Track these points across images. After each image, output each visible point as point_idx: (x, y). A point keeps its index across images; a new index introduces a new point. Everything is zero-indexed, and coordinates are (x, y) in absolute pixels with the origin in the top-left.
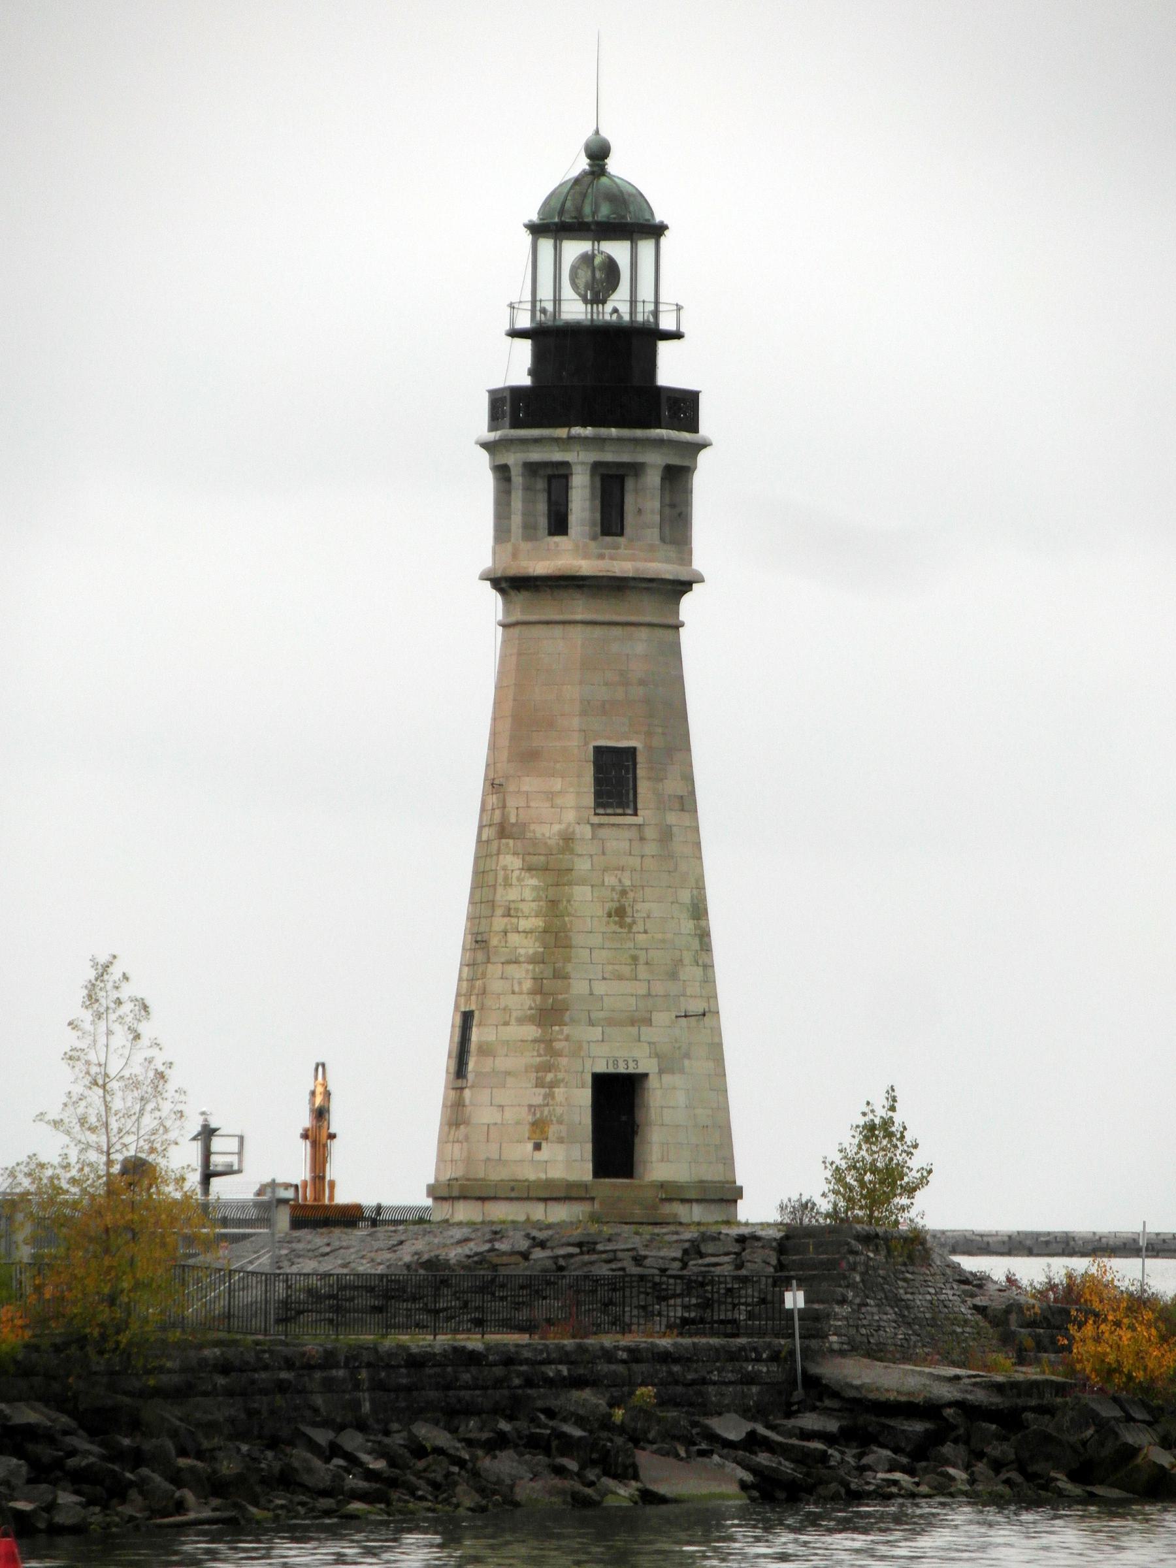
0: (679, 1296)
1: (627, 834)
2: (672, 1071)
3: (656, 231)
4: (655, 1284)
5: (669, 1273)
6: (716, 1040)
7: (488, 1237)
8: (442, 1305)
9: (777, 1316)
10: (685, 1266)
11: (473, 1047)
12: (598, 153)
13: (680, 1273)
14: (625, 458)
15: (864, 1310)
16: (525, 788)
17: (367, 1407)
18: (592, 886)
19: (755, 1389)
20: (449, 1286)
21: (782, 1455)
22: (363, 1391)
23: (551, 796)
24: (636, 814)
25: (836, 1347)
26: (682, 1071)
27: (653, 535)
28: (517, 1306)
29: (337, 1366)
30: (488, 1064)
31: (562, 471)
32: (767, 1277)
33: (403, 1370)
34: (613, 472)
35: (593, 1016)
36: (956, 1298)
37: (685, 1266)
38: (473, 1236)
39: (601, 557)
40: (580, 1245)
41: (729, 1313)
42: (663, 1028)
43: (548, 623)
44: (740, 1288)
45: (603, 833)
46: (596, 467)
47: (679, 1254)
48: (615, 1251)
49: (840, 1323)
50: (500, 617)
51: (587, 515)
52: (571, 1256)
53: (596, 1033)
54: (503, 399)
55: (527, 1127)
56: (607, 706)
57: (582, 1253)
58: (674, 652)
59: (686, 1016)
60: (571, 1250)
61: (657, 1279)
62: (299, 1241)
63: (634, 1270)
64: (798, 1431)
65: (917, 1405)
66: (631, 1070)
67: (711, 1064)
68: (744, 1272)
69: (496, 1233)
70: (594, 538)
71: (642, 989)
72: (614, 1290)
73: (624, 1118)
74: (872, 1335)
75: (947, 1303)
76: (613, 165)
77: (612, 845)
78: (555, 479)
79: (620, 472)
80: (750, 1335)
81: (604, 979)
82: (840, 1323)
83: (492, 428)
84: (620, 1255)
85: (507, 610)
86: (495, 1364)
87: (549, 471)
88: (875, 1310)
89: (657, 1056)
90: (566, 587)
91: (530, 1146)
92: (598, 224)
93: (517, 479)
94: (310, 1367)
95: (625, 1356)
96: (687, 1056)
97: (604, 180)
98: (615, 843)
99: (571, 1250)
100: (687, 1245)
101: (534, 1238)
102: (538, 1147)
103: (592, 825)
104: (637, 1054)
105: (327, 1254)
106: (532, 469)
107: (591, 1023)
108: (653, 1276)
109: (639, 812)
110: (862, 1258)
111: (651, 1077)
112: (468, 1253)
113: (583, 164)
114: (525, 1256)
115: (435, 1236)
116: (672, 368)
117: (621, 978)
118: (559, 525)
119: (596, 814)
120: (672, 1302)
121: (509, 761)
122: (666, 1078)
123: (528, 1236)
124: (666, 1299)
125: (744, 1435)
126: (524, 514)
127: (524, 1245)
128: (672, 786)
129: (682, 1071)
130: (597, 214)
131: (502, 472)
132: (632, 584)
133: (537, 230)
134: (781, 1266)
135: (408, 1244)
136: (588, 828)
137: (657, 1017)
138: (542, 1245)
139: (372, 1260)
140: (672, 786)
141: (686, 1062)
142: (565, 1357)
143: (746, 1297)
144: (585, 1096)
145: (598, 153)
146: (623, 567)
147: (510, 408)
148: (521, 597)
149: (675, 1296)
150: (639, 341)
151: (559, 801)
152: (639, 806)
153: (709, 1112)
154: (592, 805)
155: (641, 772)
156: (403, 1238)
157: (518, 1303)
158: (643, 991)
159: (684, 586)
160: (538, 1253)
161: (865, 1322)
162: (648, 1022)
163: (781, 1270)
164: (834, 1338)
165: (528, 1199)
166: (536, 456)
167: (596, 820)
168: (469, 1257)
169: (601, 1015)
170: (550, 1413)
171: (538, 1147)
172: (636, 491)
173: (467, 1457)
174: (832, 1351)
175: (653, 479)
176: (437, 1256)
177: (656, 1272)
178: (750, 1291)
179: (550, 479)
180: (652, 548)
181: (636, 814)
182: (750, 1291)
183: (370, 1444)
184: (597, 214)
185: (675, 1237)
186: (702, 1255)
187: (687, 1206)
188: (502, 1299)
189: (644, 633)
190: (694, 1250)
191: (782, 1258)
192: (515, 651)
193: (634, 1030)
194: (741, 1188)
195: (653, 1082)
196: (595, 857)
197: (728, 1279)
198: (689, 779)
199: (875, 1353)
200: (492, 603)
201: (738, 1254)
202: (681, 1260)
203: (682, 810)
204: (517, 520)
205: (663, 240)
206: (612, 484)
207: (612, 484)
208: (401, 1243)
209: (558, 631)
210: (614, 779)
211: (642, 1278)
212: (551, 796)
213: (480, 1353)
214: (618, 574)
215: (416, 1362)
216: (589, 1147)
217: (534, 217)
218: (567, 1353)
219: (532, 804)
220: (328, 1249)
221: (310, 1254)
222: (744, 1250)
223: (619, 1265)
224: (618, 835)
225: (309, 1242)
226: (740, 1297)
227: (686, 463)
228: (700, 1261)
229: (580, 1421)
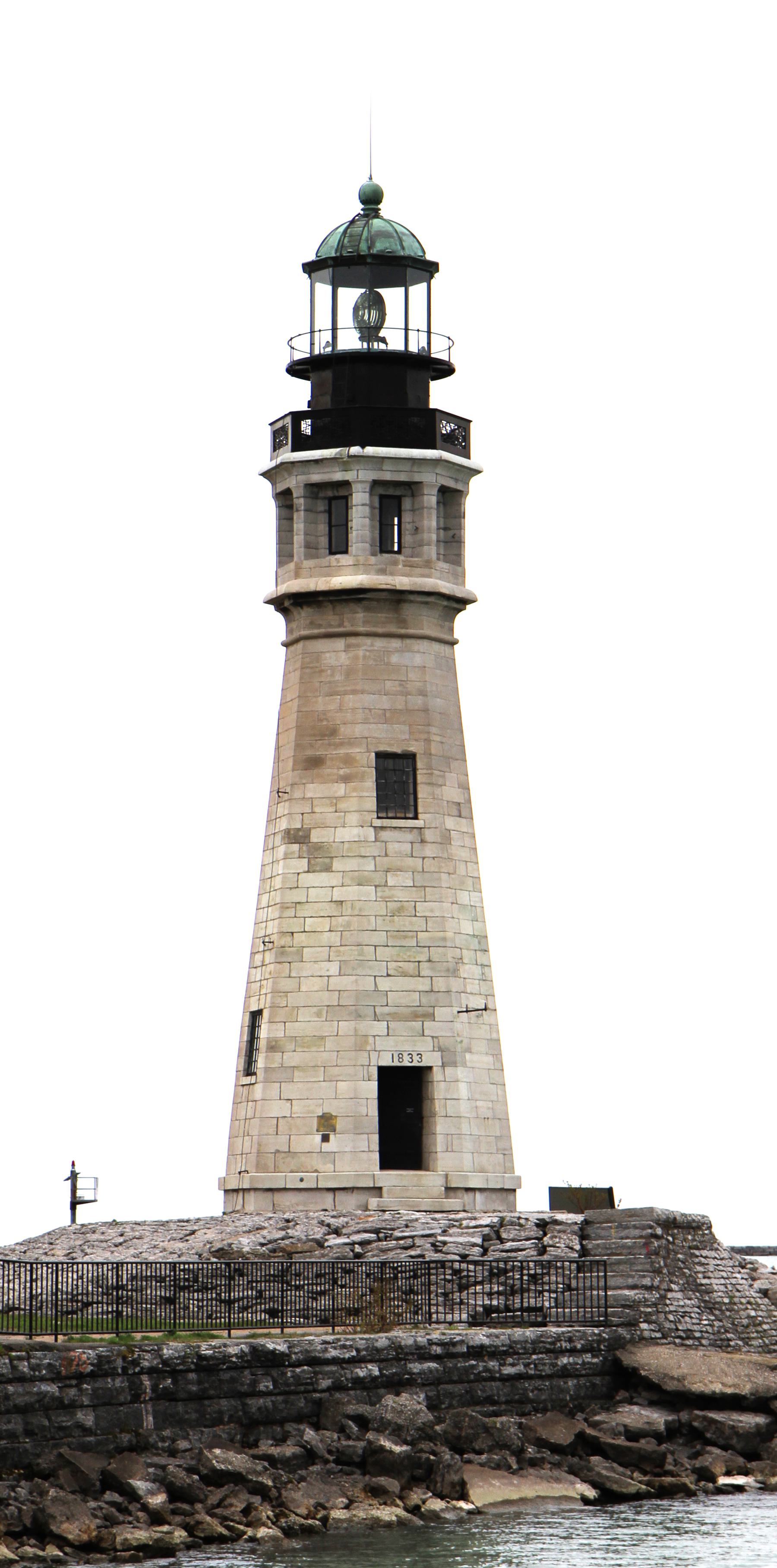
0: (481, 1283)
1: (409, 837)
2: (454, 1064)
4: (456, 1272)
5: (468, 1259)
6: (494, 1036)
7: (281, 1225)
8: (235, 1295)
9: (588, 1303)
10: (485, 1252)
11: (262, 1044)
12: (372, 199)
13: (481, 1259)
15: (670, 1295)
16: (309, 795)
17: (149, 1421)
18: (376, 886)
19: (571, 1383)
20: (242, 1275)
21: (614, 1461)
22: (145, 1402)
23: (334, 801)
24: (416, 817)
25: (646, 1334)
26: (464, 1064)
27: (431, 551)
28: (316, 1296)
29: (113, 1374)
31: (342, 492)
32: (571, 1262)
33: (192, 1376)
34: (391, 492)
35: (378, 1010)
36: (744, 1282)
37: (485, 1252)
38: (266, 1225)
39: (382, 571)
40: (377, 1231)
41: (532, 1301)
42: (447, 1023)
44: (543, 1274)
45: (385, 835)
46: (376, 484)
47: (479, 1241)
48: (412, 1237)
49: (649, 1310)
51: (367, 533)
52: (369, 1242)
53: (380, 1027)
54: (283, 429)
55: (315, 1121)
56: (388, 715)
57: (379, 1240)
58: (449, 667)
59: (467, 1011)
60: (366, 1236)
61: (456, 1266)
62: (94, 1232)
63: (431, 1256)
64: (622, 1429)
65: (742, 1398)
66: (415, 1064)
67: (490, 1059)
68: (546, 1257)
69: (288, 1221)
70: (373, 554)
71: (423, 985)
72: (415, 1277)
73: (409, 1110)
74: (680, 1322)
75: (738, 1287)
76: (385, 209)
77: (393, 847)
78: (332, 499)
79: (398, 492)
80: (558, 1324)
81: (388, 975)
82: (649, 1310)
84: (418, 1242)
85: (289, 631)
86: (299, 1364)
87: (330, 493)
88: (679, 1295)
89: (441, 1050)
90: (347, 601)
91: (318, 1138)
92: (373, 256)
93: (300, 502)
94: (81, 1377)
95: (438, 1350)
96: (469, 1050)
97: (376, 222)
98: (397, 845)
99: (366, 1236)
100: (486, 1230)
101: (329, 1225)
102: (325, 1139)
103: (375, 827)
104: (420, 1048)
105: (121, 1244)
106: (314, 490)
107: (376, 1018)
108: (453, 1261)
109: (420, 816)
110: (664, 1242)
111: (435, 1069)
112: (262, 1241)
113: (357, 208)
114: (320, 1244)
115: (228, 1225)
117: (405, 974)
118: (338, 544)
119: (378, 818)
120: (472, 1290)
121: (293, 770)
122: (449, 1070)
123: (322, 1223)
124: (467, 1287)
125: (573, 1437)
126: (306, 534)
127: (318, 1233)
128: (451, 793)
129: (464, 1064)
131: (284, 499)
132: (412, 597)
133: (310, 268)
134: (584, 1252)
135: (199, 1233)
136: (372, 829)
137: (439, 1012)
138: (337, 1232)
139: (165, 1250)
140: (451, 793)
141: (468, 1056)
142: (374, 1355)
143: (549, 1284)
144: (372, 1087)
145: (372, 199)
146: (402, 582)
147: (287, 432)
148: (304, 614)
149: (476, 1283)
151: (342, 806)
152: (420, 810)
153: (490, 1105)
154: (375, 808)
155: (420, 778)
156: (196, 1228)
157: (317, 1293)
158: (428, 988)
159: (461, 603)
160: (334, 1241)
161: (672, 1308)
162: (432, 1017)
163: (584, 1255)
164: (644, 1326)
165: (333, 1190)
166: (316, 477)
167: (378, 823)
168: (262, 1245)
169: (386, 1010)
170: (363, 1422)
171: (325, 1139)
172: (413, 510)
173: (270, 1483)
174: (642, 1338)
175: (431, 499)
176: (230, 1245)
177: (457, 1258)
178: (553, 1278)
180: (428, 564)
181: (416, 817)
182: (553, 1278)
183: (151, 1470)
185: (473, 1223)
186: (502, 1241)
187: (471, 1194)
188: (298, 1288)
189: (424, 645)
190: (494, 1234)
191: (584, 1242)
192: (298, 665)
193: (417, 1025)
194: (519, 1178)
195: (437, 1075)
196: (377, 858)
197: (532, 1265)
198: (465, 787)
199: (687, 1339)
200: (276, 624)
201: (540, 1239)
202: (482, 1246)
203: (460, 816)
204: (298, 539)
205: (433, 281)
206: (392, 499)
207: (392, 499)
208: (193, 1232)
209: (340, 643)
210: (397, 784)
211: (442, 1264)
212: (334, 801)
213: (282, 1354)
214: (398, 588)
215: (208, 1367)
216: (376, 1138)
217: (311, 257)
218: (378, 1350)
219: (316, 810)
220: (121, 1240)
221: (104, 1245)
222: (545, 1234)
223: (418, 1252)
224: (398, 837)
225: (103, 1233)
226: (543, 1283)
227: (459, 487)
228: (500, 1247)
229: (398, 1432)
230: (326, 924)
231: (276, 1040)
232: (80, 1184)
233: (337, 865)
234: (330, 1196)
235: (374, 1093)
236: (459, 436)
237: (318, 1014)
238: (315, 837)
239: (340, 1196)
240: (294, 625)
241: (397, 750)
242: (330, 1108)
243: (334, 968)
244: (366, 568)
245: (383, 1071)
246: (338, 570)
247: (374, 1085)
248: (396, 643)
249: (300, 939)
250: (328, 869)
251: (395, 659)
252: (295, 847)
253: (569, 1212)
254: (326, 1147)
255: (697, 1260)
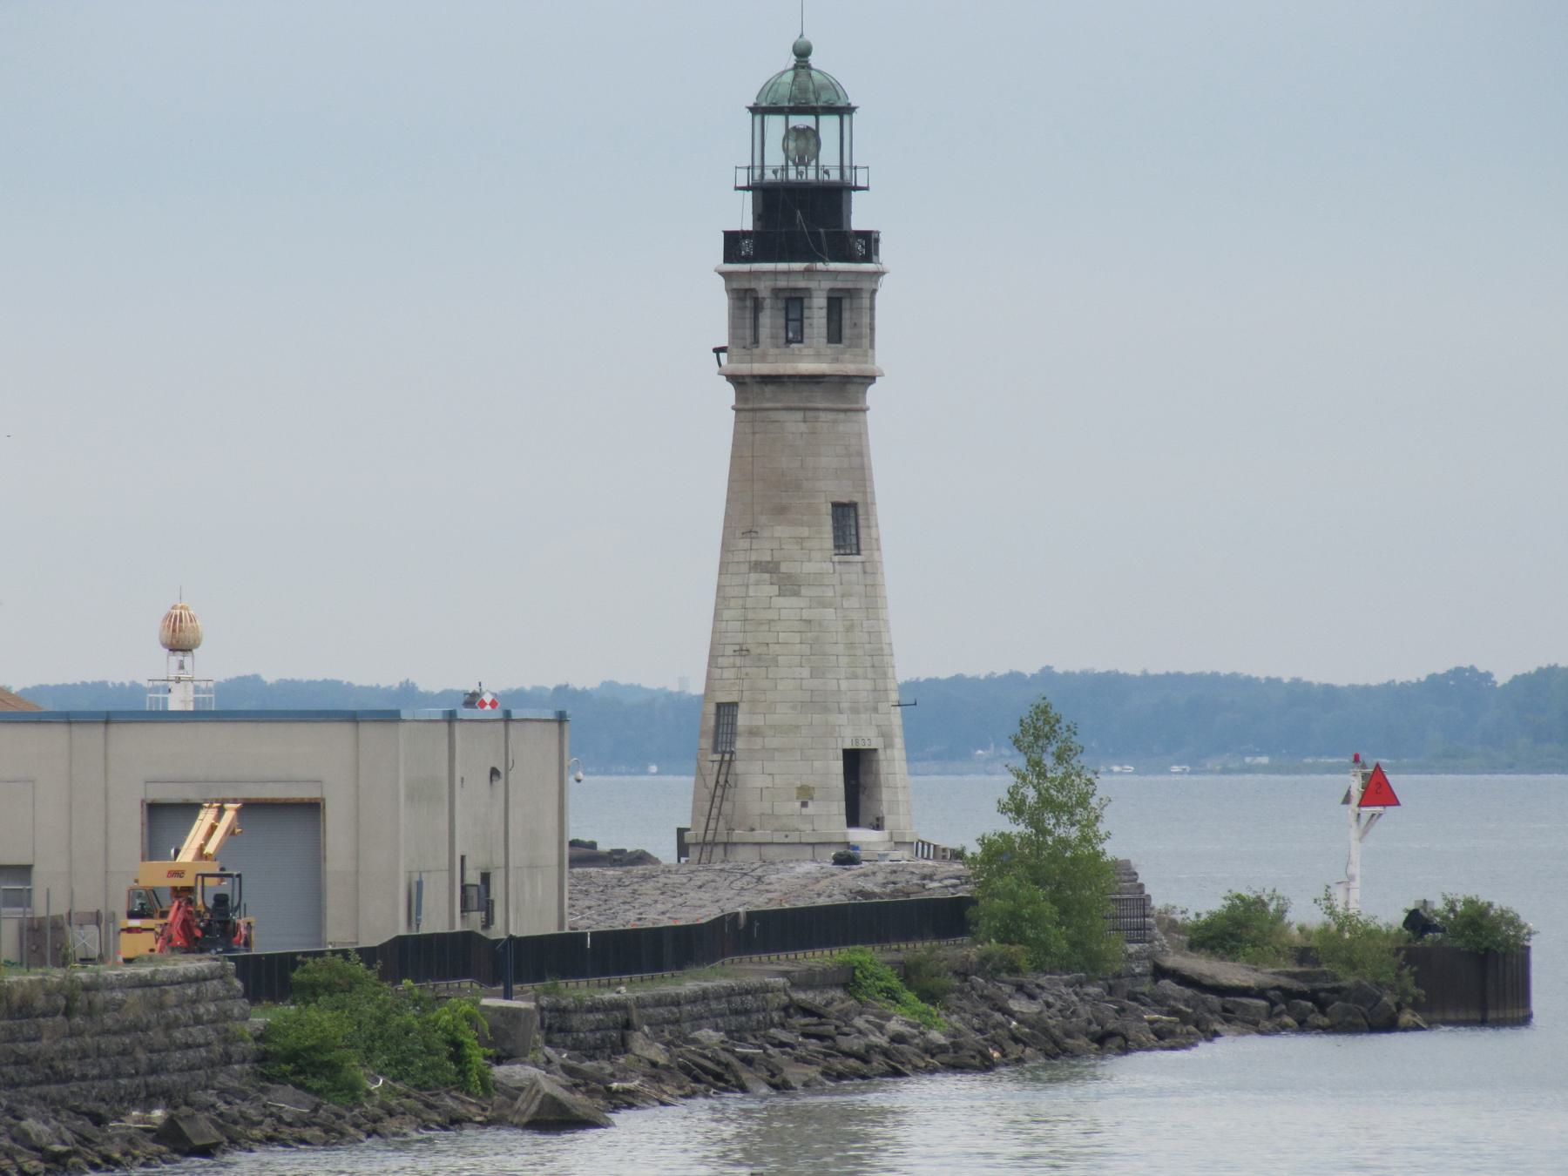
3: (848, 110)
12: (802, 53)
14: (850, 285)
16: (776, 535)
23: (800, 540)
30: (758, 743)
39: (836, 360)
43: (791, 409)
50: (733, 402)
76: (813, 60)
83: (727, 259)
87: (787, 295)
91: (798, 804)
102: (804, 804)
107: (840, 712)
116: (861, 215)
130: (804, 99)
133: (759, 110)
145: (802, 53)
150: (834, 197)
151: (807, 544)
159: (871, 379)
165: (813, 844)
171: (804, 804)
172: (851, 309)
179: (789, 300)
184: (804, 99)
195: (881, 755)
209: (799, 415)
212: (800, 540)
230: (797, 638)
231: (758, 727)
232: (754, 775)
233: (804, 591)
234: (809, 849)
235: (841, 770)
236: (868, 244)
237: (794, 708)
238: (784, 568)
239: (818, 849)
240: (746, 400)
241: (845, 500)
242: (809, 781)
243: (806, 673)
244: (818, 356)
245: (846, 752)
246: (801, 358)
247: (841, 763)
248: (842, 416)
249: (774, 649)
250: (796, 594)
251: (841, 428)
252: (767, 576)
253: (907, 938)
254: (805, 811)
255: (946, 1058)
